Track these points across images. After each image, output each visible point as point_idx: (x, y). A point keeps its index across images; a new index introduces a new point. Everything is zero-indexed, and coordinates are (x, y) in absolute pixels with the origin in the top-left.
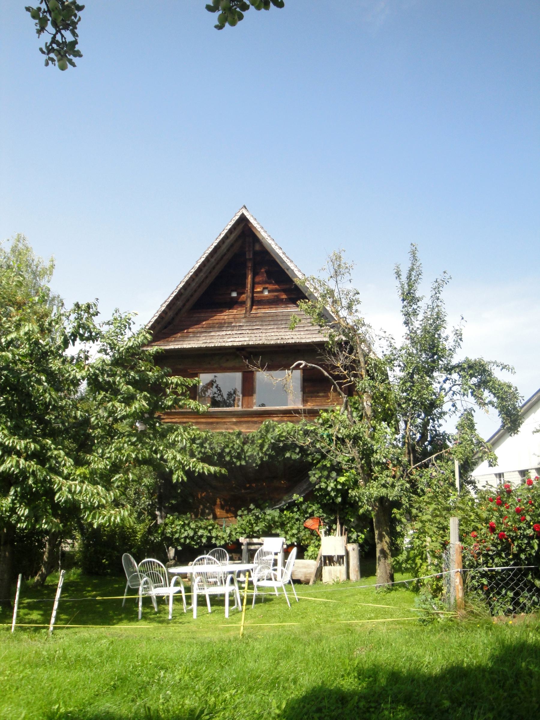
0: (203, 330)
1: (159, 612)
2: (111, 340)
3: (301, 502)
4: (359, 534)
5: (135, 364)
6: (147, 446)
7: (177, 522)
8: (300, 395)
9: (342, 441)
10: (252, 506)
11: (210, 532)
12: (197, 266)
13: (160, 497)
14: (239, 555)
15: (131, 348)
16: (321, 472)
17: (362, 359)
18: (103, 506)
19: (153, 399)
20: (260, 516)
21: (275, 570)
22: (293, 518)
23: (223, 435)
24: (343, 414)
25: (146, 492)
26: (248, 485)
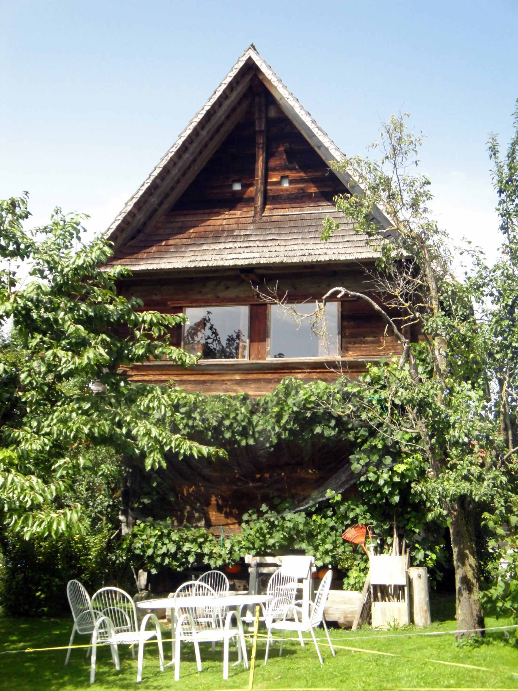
0: (190, 241)
1: (122, 671)
2: (51, 256)
3: (338, 502)
4: (428, 553)
5: (88, 293)
6: (106, 415)
7: (149, 531)
8: (337, 339)
9: (402, 409)
10: (264, 508)
11: (200, 546)
12: (180, 142)
13: (126, 494)
14: (244, 582)
15: (81, 267)
16: (368, 457)
17: (432, 285)
18: (39, 507)
19: (115, 345)
20: (276, 523)
21: (300, 605)
22: (325, 525)
23: (221, 400)
24: (402, 368)
25: (105, 486)
26: (258, 476)
